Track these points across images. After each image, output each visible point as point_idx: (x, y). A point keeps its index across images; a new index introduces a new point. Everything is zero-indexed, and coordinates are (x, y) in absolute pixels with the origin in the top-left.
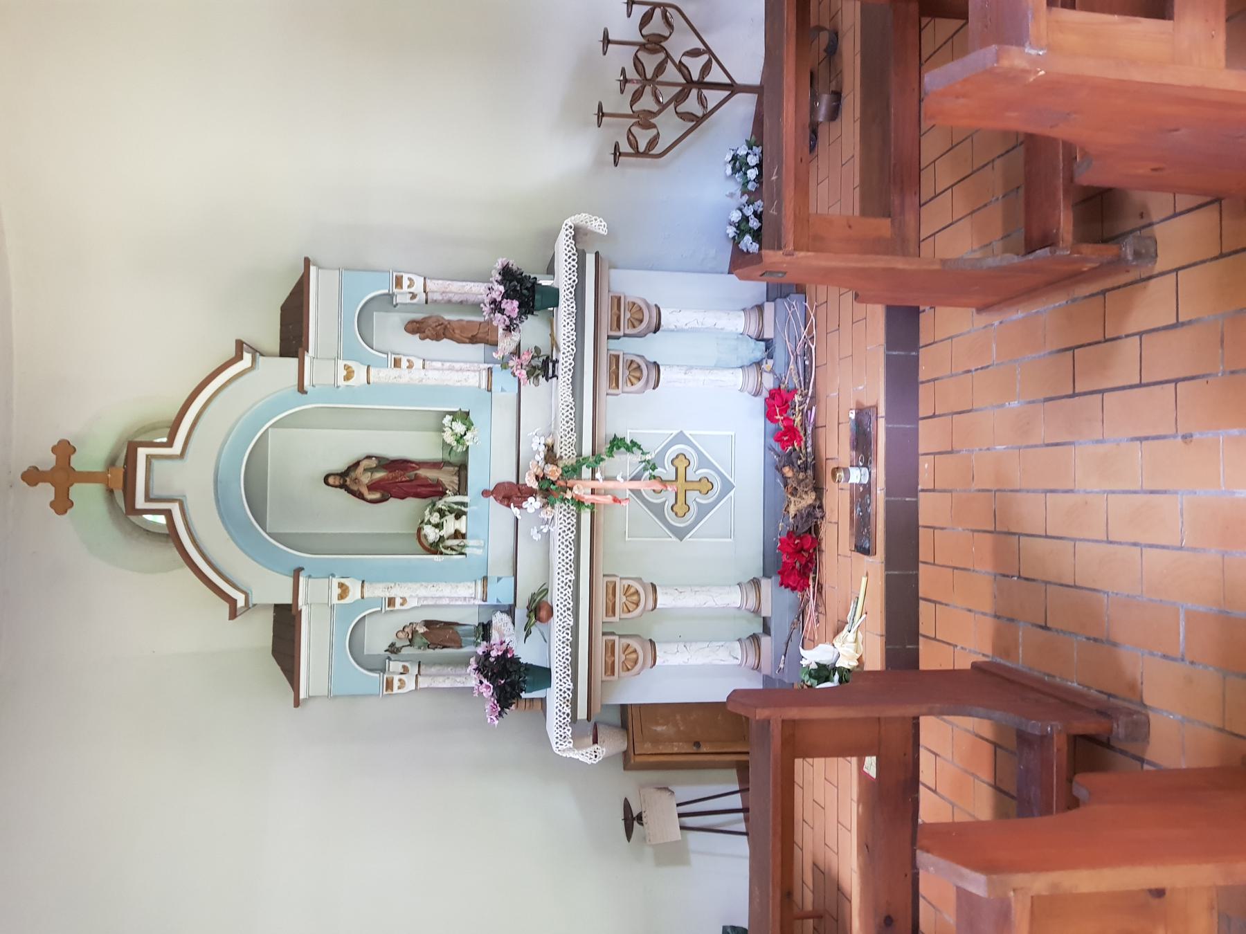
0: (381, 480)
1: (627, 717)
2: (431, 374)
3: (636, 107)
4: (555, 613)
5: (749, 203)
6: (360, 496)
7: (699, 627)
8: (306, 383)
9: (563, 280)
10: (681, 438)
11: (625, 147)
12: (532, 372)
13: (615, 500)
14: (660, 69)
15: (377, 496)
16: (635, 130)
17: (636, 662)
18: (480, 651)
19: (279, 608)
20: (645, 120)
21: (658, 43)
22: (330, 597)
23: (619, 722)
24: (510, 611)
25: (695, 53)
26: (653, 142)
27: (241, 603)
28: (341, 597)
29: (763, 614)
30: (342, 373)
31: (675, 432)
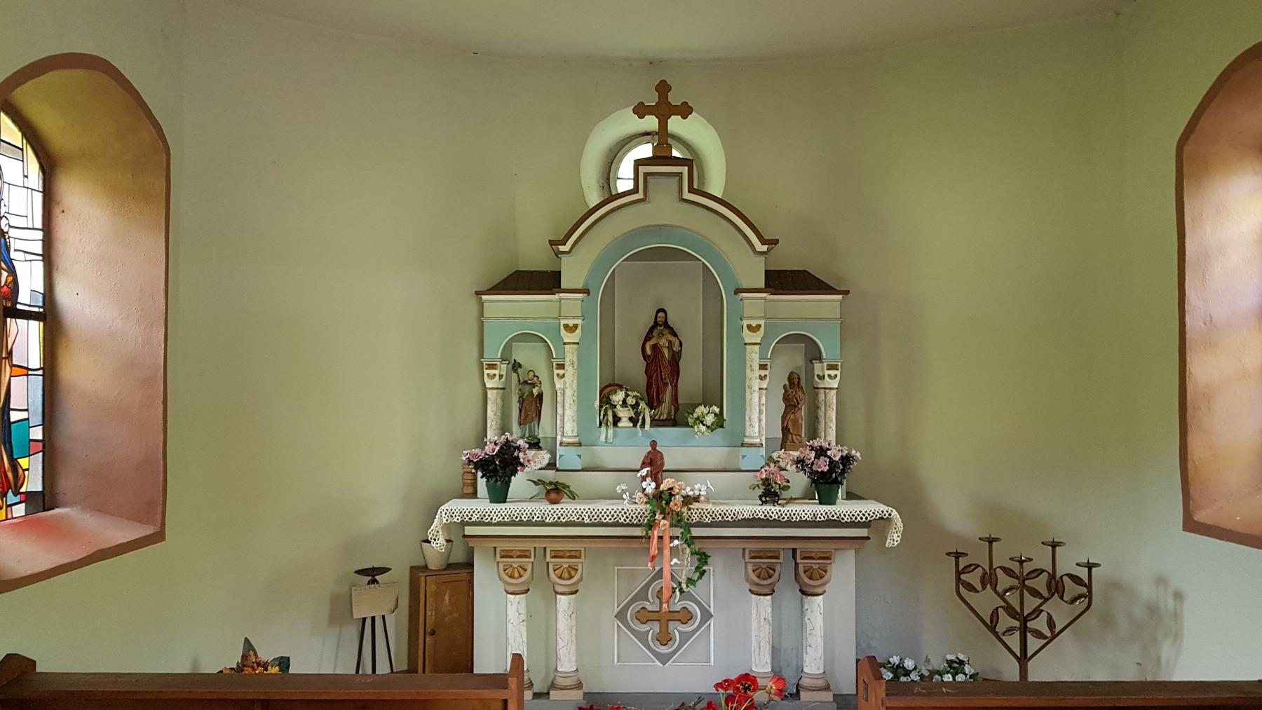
0: (663, 355)
1: (460, 571)
2: (756, 395)
3: (999, 572)
4: (555, 507)
5: (922, 676)
6: (648, 338)
7: (541, 628)
8: (745, 295)
9: (843, 508)
10: (707, 615)
11: (963, 562)
12: (766, 482)
13: (653, 558)
14: (1035, 593)
15: (649, 352)
16: (979, 571)
17: (511, 577)
18: (521, 442)
19: (557, 275)
20: (989, 579)
21: (1057, 590)
22: (566, 317)
23: (451, 561)
24: (551, 465)
25: (1051, 623)
26: (971, 588)
27: (562, 248)
28: (566, 326)
29: (552, 693)
30: (754, 323)
31: (712, 610)
